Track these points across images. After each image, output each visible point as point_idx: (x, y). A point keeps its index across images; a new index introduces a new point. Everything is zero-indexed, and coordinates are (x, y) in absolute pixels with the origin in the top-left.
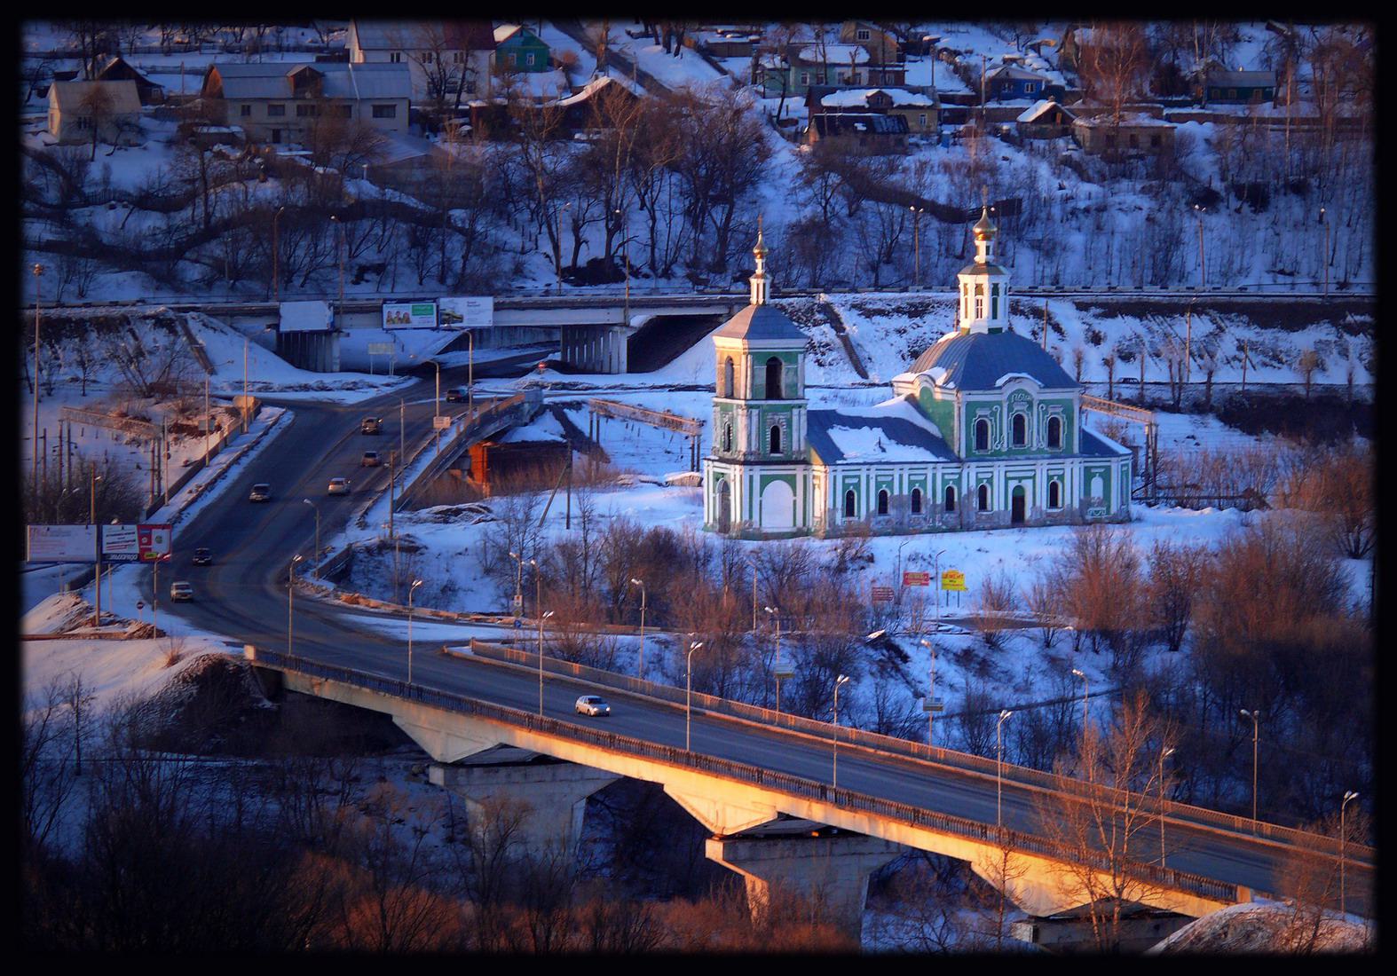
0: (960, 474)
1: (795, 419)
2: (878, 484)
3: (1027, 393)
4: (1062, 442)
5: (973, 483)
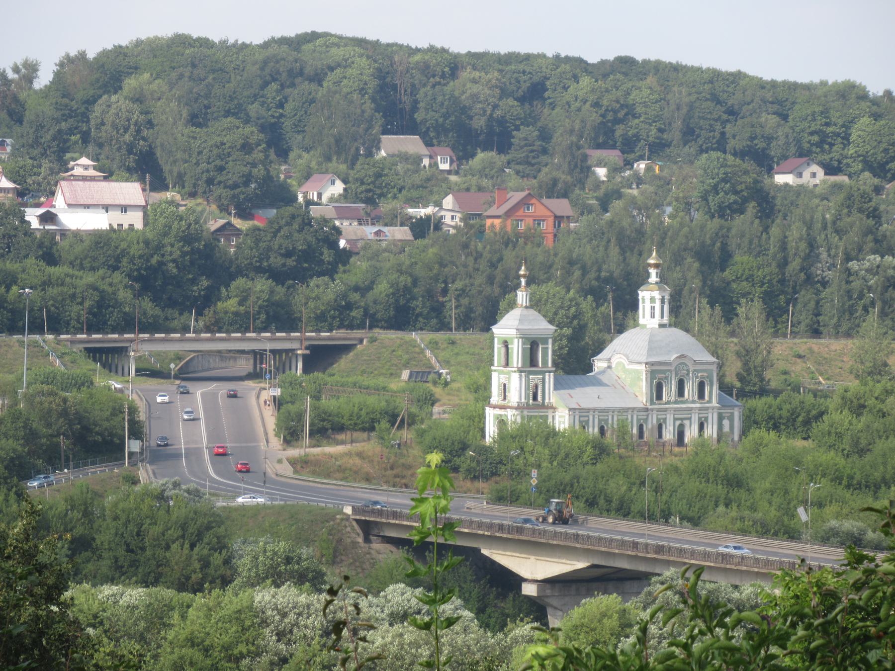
0: (648, 416)
1: (547, 380)
2: (600, 421)
3: (686, 365)
4: (707, 397)
5: (655, 421)
